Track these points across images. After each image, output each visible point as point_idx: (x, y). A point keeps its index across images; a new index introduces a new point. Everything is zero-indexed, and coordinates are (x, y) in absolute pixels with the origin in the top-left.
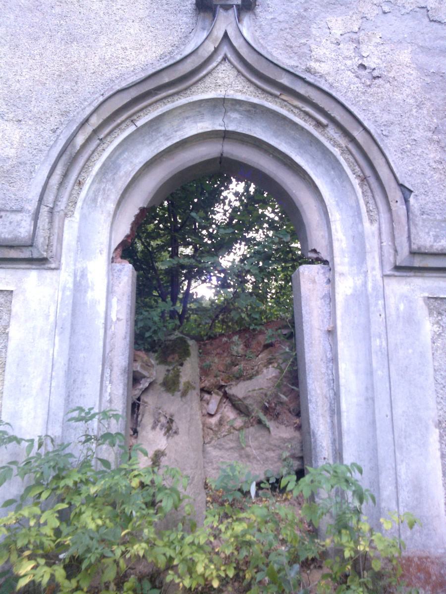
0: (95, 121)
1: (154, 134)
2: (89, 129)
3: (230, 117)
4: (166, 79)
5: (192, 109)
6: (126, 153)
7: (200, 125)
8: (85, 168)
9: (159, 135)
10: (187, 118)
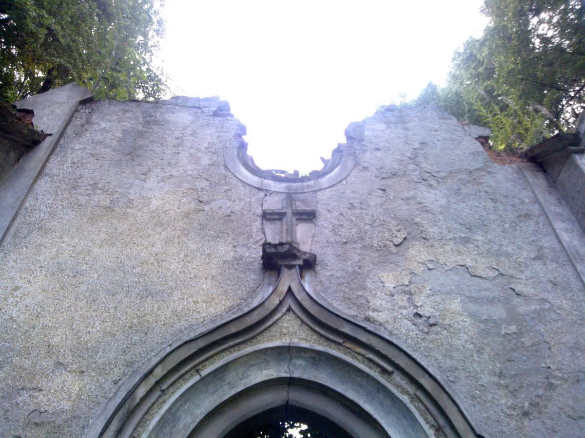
0: (159, 372)
1: (218, 383)
2: (152, 380)
3: (295, 364)
4: (233, 329)
5: (257, 357)
6: (188, 404)
7: (265, 372)
8: (142, 422)
9: (223, 383)
10: (252, 366)
